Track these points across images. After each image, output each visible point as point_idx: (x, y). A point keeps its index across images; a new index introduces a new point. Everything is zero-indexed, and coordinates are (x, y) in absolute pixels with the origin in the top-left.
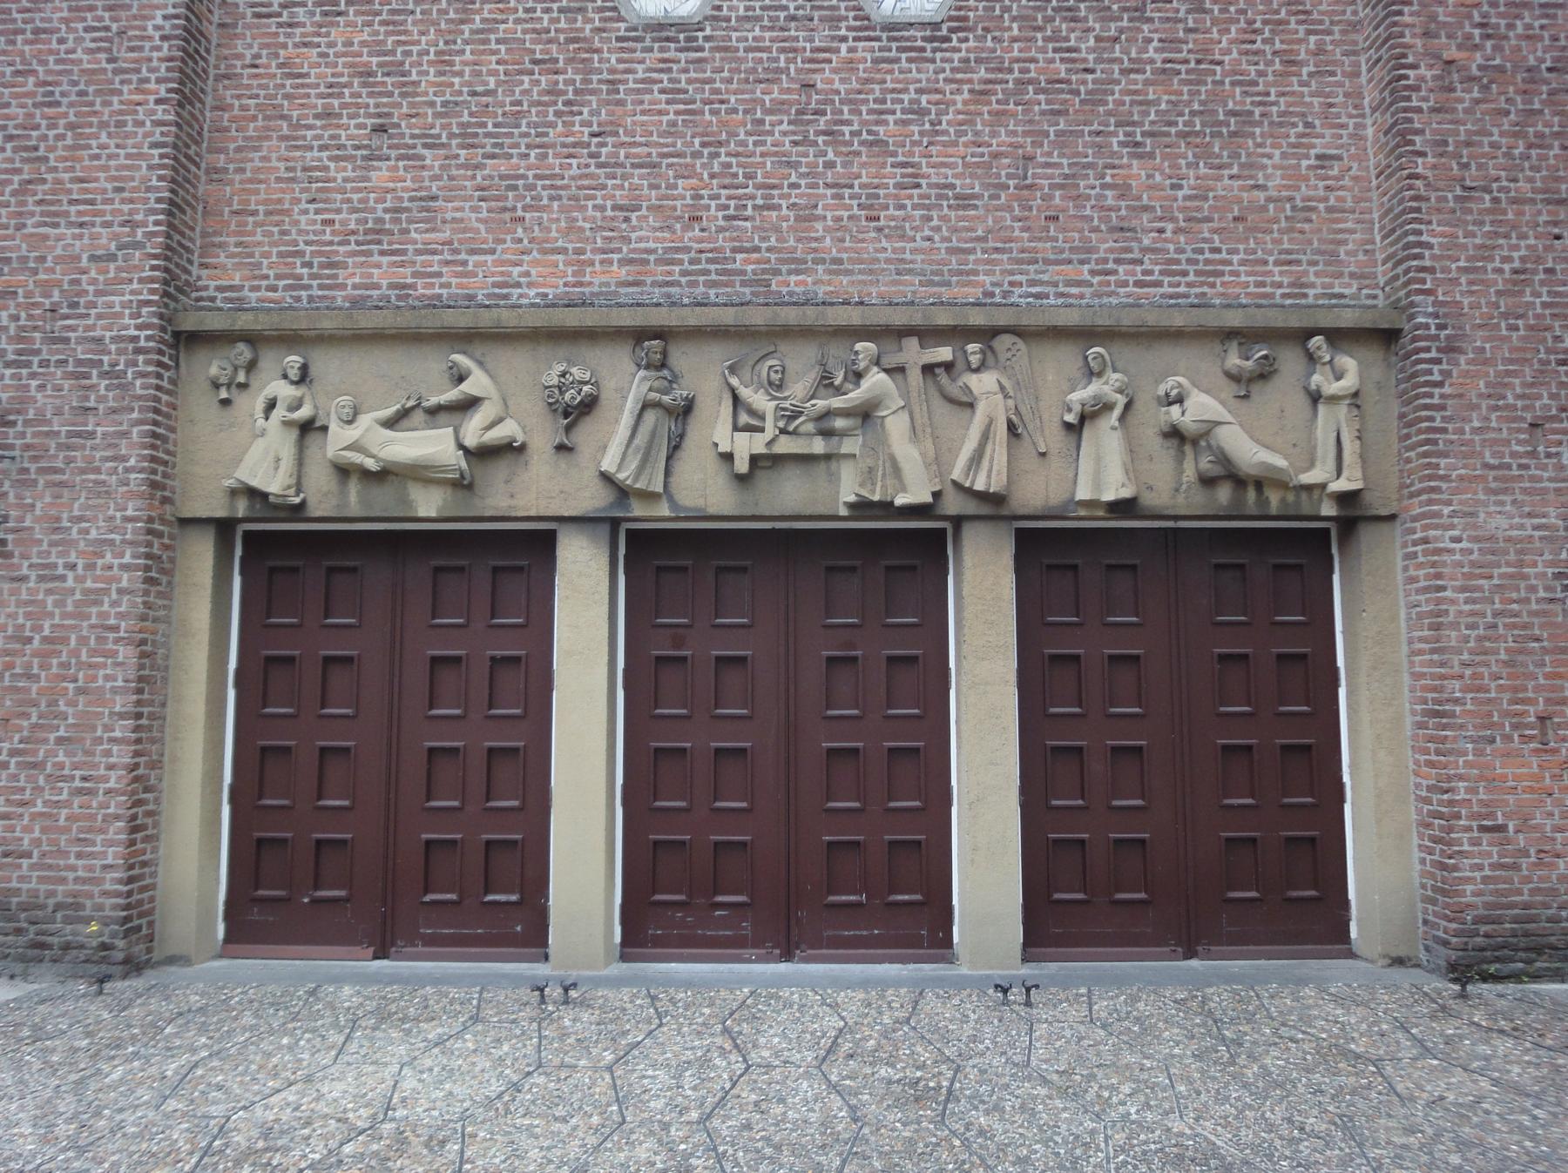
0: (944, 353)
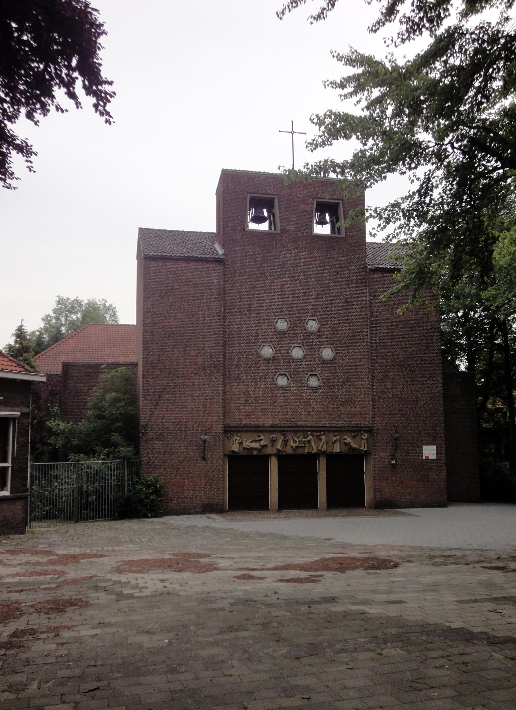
0: (319, 434)
